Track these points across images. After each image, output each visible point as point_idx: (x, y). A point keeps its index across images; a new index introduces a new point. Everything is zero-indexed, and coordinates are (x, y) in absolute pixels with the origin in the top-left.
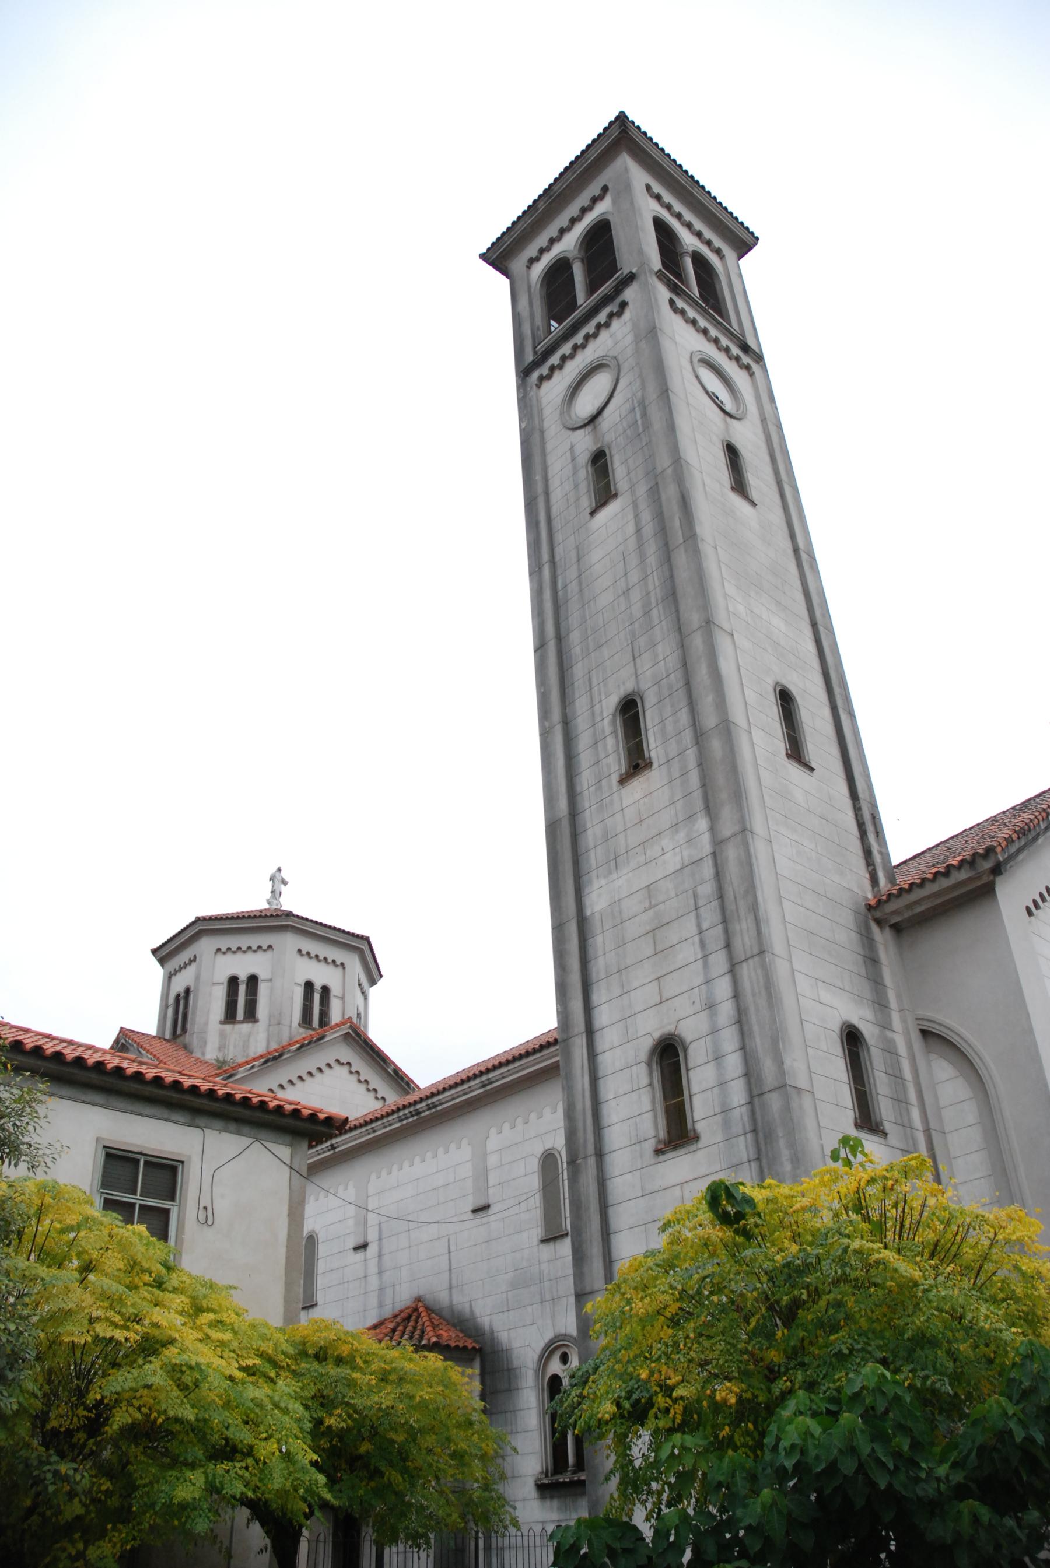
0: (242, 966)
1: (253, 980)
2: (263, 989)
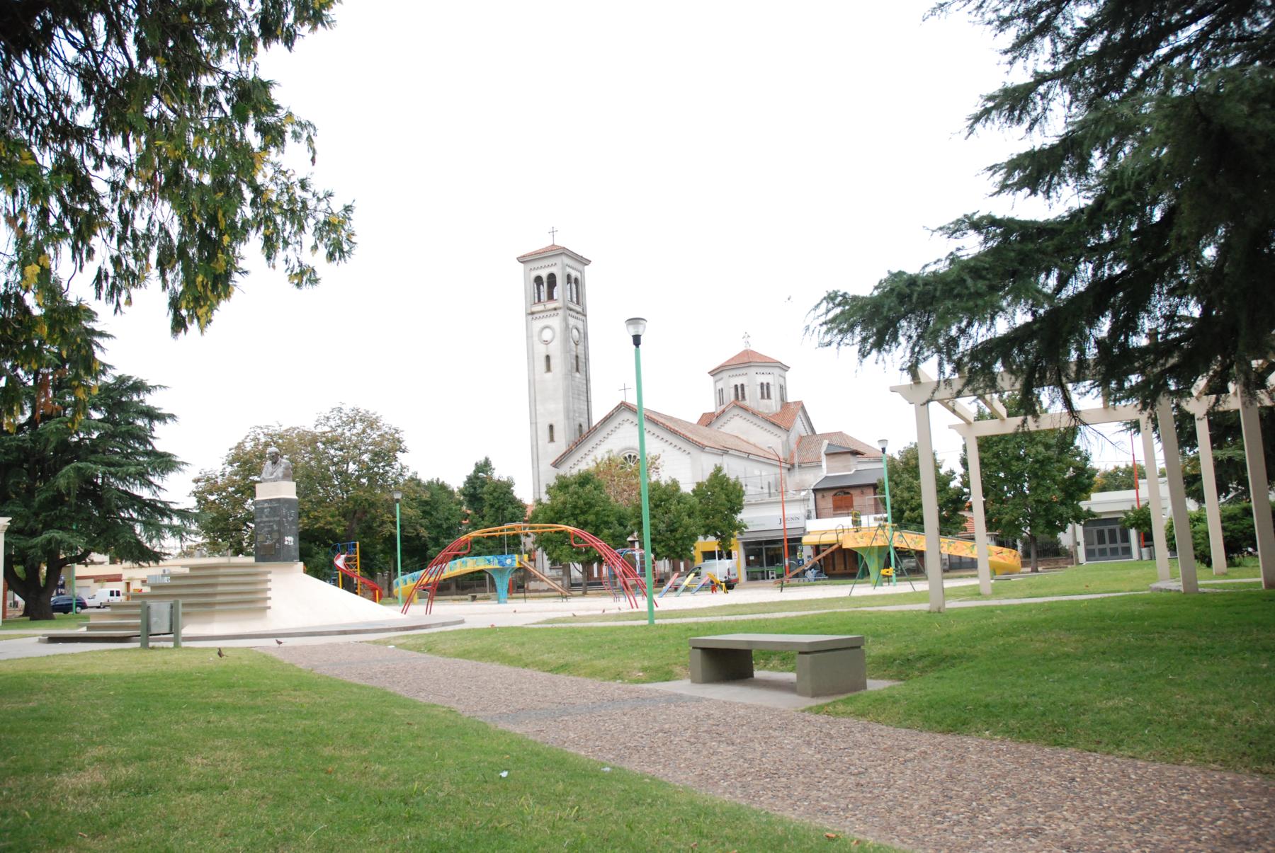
0: (739, 381)
1: (742, 385)
2: (746, 389)
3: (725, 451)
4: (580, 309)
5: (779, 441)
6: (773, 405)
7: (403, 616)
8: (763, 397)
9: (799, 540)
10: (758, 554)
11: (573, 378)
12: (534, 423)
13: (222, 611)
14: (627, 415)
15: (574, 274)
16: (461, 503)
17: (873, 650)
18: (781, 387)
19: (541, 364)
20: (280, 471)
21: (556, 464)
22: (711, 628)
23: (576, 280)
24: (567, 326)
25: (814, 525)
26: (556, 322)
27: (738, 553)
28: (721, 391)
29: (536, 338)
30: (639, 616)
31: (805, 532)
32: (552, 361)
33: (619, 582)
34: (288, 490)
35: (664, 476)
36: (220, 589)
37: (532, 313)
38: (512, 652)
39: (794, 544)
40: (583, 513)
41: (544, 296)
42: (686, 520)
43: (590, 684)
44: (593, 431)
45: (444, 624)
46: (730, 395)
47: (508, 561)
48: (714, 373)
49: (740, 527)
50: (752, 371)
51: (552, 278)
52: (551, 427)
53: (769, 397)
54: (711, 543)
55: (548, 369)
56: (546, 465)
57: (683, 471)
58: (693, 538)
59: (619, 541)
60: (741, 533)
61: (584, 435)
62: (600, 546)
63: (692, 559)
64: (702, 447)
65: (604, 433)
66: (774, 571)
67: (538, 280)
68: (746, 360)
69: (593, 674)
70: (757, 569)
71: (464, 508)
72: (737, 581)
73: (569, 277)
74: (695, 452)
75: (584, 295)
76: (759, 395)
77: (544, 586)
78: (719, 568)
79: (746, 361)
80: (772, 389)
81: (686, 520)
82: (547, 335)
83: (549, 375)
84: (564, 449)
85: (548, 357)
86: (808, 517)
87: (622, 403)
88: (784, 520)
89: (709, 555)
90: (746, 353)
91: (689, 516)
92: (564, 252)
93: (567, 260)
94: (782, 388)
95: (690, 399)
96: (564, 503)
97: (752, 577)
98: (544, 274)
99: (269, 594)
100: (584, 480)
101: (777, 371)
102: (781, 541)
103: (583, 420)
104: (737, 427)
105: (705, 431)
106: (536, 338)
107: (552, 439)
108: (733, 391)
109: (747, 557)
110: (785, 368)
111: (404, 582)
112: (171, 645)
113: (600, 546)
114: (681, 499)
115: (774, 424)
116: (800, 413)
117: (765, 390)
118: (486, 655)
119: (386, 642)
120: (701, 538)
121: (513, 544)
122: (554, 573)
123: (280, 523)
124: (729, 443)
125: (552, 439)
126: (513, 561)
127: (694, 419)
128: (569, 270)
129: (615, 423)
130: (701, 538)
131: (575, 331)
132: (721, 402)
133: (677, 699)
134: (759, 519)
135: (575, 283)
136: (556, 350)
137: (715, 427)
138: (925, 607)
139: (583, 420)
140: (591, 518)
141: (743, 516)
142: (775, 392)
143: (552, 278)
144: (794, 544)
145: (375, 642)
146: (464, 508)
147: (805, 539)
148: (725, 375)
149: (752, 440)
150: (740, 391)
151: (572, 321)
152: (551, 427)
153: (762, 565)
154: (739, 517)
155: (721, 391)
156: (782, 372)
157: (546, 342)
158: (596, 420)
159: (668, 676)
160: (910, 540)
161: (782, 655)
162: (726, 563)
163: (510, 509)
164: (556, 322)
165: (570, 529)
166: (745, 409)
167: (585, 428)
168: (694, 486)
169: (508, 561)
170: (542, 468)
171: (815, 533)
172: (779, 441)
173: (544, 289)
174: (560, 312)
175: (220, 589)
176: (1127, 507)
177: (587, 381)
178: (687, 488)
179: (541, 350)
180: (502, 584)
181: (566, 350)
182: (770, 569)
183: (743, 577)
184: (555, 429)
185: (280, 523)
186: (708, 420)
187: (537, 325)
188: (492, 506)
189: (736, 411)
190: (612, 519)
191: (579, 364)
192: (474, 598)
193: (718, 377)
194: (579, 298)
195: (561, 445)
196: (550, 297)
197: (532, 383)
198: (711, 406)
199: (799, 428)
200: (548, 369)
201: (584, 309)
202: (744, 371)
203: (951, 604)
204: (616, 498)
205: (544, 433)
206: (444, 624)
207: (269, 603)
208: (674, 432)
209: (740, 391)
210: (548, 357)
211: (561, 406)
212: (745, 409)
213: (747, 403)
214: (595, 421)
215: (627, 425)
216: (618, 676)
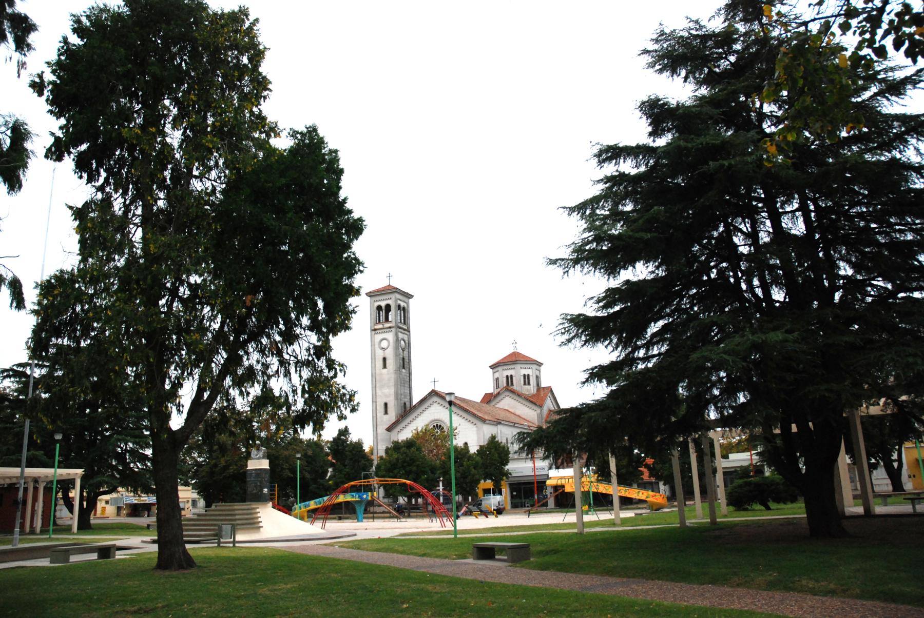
0: (509, 373)
2: (514, 378)
3: (498, 423)
4: (405, 327)
5: (535, 413)
6: (531, 389)
7: (323, 531)
8: (525, 384)
9: (545, 482)
10: (519, 491)
11: (401, 372)
12: (374, 402)
13: (243, 529)
14: (435, 399)
15: (402, 304)
16: (327, 454)
17: (533, 549)
18: (537, 377)
19: (380, 363)
20: (261, 454)
21: (389, 429)
22: (482, 539)
23: (404, 308)
24: (397, 338)
25: (553, 473)
26: (390, 336)
27: (506, 491)
28: (497, 379)
29: (377, 346)
30: (448, 532)
31: (548, 478)
32: (387, 362)
33: (430, 508)
34: (265, 464)
35: (459, 442)
36: (237, 517)
37: (375, 330)
38: (401, 549)
39: (541, 484)
40: (409, 465)
41: (382, 318)
42: (473, 471)
43: (437, 560)
44: (413, 408)
45: (349, 536)
46: (503, 383)
47: (365, 496)
48: (493, 367)
49: (507, 474)
50: (519, 366)
51: (388, 307)
52: (386, 405)
53: (529, 384)
54: (489, 484)
55: (385, 366)
56: (382, 430)
57: (470, 436)
58: (478, 482)
59: (431, 485)
60: (508, 478)
61: (407, 411)
62: (418, 487)
63: (476, 495)
64: (484, 421)
65: (420, 410)
66: (528, 502)
67: (379, 308)
68: (514, 359)
69: (437, 557)
70: (517, 501)
71: (330, 458)
72: (504, 509)
73: (399, 306)
74: (479, 424)
75: (409, 318)
76: (522, 382)
77: (381, 509)
78: (493, 501)
79: (515, 359)
80: (531, 378)
81: (473, 471)
82: (384, 344)
83: (385, 370)
84: (394, 419)
85: (384, 359)
86: (550, 468)
87: (433, 391)
88: (534, 469)
89: (487, 492)
90: (515, 354)
91: (475, 468)
92: (396, 291)
93: (398, 296)
94: (538, 378)
95: (475, 385)
96: (397, 459)
97: (515, 506)
98: (383, 304)
99: (260, 520)
100: (409, 444)
101: (535, 367)
102: (533, 483)
103: (407, 400)
104: (507, 403)
105: (486, 407)
106: (377, 346)
107: (386, 413)
108: (505, 379)
109: (512, 493)
110: (540, 364)
111: (299, 507)
112: (231, 545)
113: (418, 487)
114: (470, 457)
115: (532, 402)
116: (550, 394)
117: (526, 379)
118: (387, 550)
119: (332, 545)
120: (482, 481)
121: (368, 488)
122: (386, 500)
123: (261, 482)
124: (502, 415)
125: (386, 413)
126: (367, 496)
127: (478, 399)
128: (399, 302)
129: (428, 403)
130: (482, 481)
131: (402, 342)
132: (498, 387)
133: (469, 564)
134: (521, 467)
135: (404, 311)
136: (390, 354)
137: (493, 404)
138: (576, 531)
139: (407, 400)
140: (414, 469)
141: (510, 467)
142: (533, 381)
143: (388, 307)
144: (541, 484)
145: (325, 545)
146: (330, 458)
147: (548, 482)
148: (500, 369)
149: (518, 413)
150: (510, 379)
151: (401, 336)
152: (386, 405)
153: (521, 498)
154: (507, 467)
155: (497, 379)
156: (538, 367)
157: (384, 349)
158: (415, 401)
159: (465, 557)
160: (602, 488)
161: (502, 549)
162: (498, 498)
163: (363, 462)
164: (390, 336)
165: (408, 482)
166: (513, 392)
167: (408, 408)
168: (478, 448)
169: (365, 496)
170: (379, 431)
171: (555, 478)
172: (535, 413)
173: (383, 313)
174: (393, 330)
175: (237, 517)
176: (745, 464)
177: (410, 374)
178: (473, 449)
179: (380, 354)
180: (360, 510)
181: (397, 355)
182: (527, 501)
183: (509, 506)
184: (389, 406)
185: (261, 482)
186: (489, 399)
187: (378, 337)
188: (351, 459)
189: (507, 393)
190: (427, 469)
191: (405, 363)
192: (340, 519)
193: (496, 370)
194: (406, 320)
195: (392, 416)
196: (387, 320)
197: (374, 376)
198: (490, 389)
199: (549, 404)
200: (385, 366)
201: (409, 328)
202: (512, 366)
203: (586, 530)
204: (429, 454)
205: (381, 409)
206: (349, 536)
207: (261, 524)
208: (466, 411)
209: (510, 379)
210: (384, 359)
211: (392, 391)
212: (513, 392)
213: (515, 387)
214: (415, 402)
215: (435, 405)
216: (446, 557)
